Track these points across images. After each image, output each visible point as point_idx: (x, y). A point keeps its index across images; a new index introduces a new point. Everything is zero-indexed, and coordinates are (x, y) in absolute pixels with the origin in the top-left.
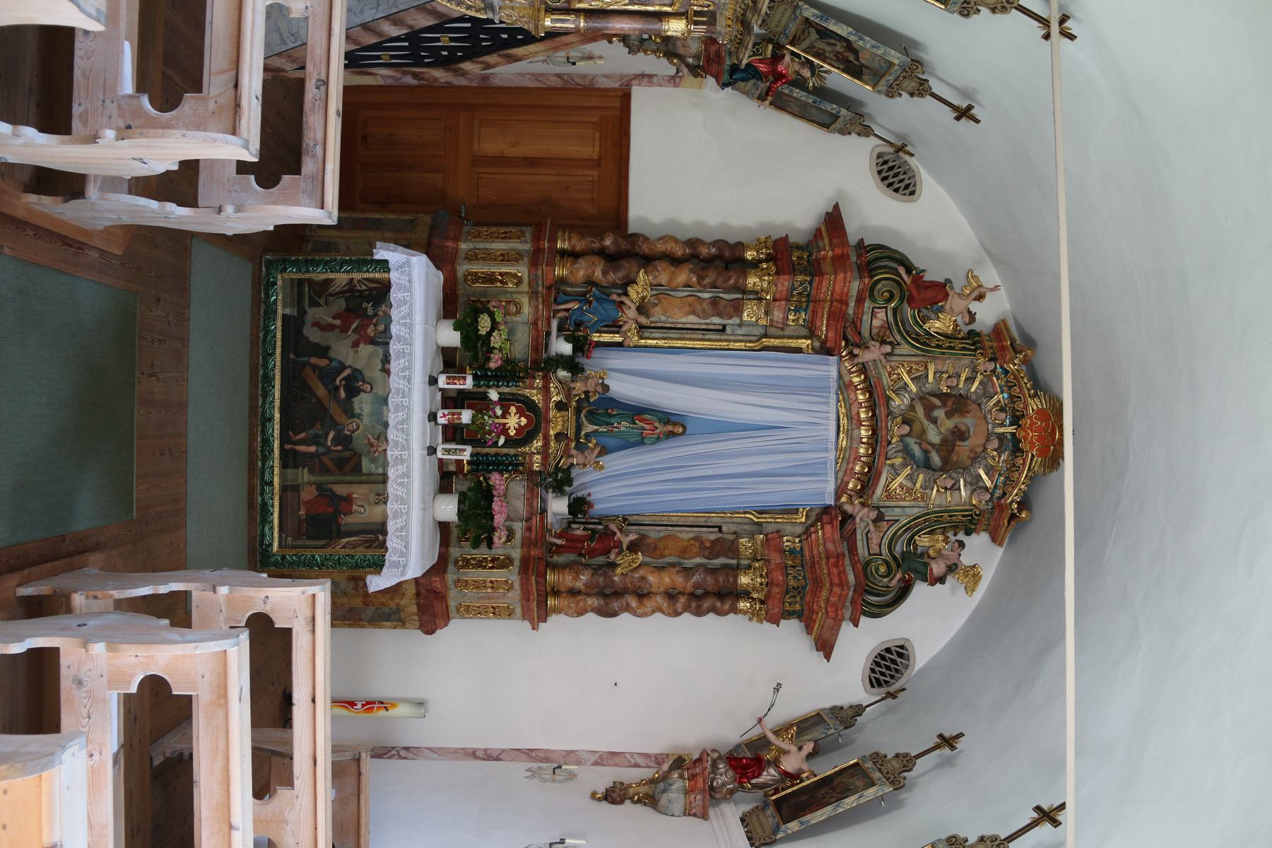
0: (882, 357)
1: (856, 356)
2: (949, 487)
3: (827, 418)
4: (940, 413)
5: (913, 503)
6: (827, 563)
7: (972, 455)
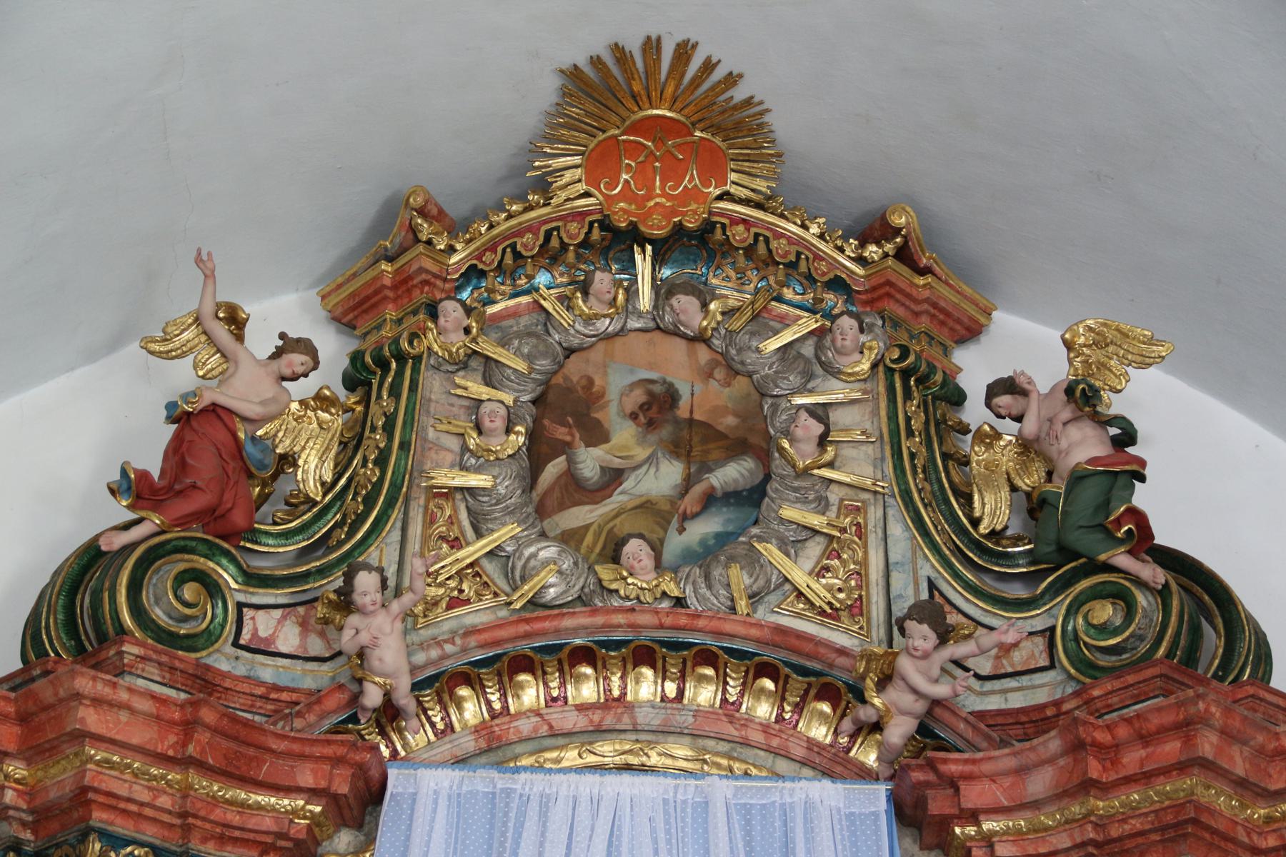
0: (395, 606)
1: (387, 695)
2: (818, 429)
3: (595, 802)
4: (590, 461)
5: (874, 540)
6: (1104, 789)
7: (719, 373)
